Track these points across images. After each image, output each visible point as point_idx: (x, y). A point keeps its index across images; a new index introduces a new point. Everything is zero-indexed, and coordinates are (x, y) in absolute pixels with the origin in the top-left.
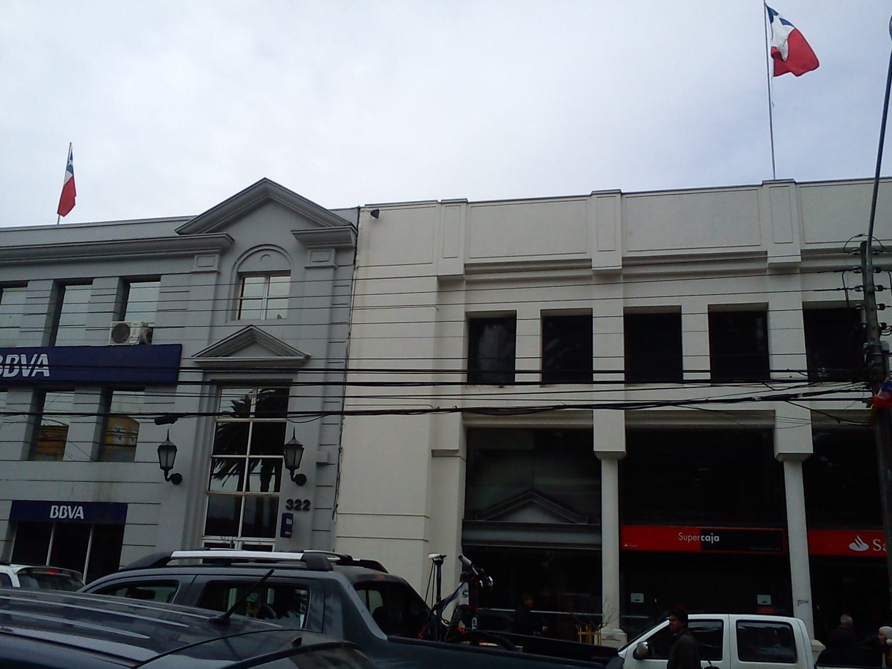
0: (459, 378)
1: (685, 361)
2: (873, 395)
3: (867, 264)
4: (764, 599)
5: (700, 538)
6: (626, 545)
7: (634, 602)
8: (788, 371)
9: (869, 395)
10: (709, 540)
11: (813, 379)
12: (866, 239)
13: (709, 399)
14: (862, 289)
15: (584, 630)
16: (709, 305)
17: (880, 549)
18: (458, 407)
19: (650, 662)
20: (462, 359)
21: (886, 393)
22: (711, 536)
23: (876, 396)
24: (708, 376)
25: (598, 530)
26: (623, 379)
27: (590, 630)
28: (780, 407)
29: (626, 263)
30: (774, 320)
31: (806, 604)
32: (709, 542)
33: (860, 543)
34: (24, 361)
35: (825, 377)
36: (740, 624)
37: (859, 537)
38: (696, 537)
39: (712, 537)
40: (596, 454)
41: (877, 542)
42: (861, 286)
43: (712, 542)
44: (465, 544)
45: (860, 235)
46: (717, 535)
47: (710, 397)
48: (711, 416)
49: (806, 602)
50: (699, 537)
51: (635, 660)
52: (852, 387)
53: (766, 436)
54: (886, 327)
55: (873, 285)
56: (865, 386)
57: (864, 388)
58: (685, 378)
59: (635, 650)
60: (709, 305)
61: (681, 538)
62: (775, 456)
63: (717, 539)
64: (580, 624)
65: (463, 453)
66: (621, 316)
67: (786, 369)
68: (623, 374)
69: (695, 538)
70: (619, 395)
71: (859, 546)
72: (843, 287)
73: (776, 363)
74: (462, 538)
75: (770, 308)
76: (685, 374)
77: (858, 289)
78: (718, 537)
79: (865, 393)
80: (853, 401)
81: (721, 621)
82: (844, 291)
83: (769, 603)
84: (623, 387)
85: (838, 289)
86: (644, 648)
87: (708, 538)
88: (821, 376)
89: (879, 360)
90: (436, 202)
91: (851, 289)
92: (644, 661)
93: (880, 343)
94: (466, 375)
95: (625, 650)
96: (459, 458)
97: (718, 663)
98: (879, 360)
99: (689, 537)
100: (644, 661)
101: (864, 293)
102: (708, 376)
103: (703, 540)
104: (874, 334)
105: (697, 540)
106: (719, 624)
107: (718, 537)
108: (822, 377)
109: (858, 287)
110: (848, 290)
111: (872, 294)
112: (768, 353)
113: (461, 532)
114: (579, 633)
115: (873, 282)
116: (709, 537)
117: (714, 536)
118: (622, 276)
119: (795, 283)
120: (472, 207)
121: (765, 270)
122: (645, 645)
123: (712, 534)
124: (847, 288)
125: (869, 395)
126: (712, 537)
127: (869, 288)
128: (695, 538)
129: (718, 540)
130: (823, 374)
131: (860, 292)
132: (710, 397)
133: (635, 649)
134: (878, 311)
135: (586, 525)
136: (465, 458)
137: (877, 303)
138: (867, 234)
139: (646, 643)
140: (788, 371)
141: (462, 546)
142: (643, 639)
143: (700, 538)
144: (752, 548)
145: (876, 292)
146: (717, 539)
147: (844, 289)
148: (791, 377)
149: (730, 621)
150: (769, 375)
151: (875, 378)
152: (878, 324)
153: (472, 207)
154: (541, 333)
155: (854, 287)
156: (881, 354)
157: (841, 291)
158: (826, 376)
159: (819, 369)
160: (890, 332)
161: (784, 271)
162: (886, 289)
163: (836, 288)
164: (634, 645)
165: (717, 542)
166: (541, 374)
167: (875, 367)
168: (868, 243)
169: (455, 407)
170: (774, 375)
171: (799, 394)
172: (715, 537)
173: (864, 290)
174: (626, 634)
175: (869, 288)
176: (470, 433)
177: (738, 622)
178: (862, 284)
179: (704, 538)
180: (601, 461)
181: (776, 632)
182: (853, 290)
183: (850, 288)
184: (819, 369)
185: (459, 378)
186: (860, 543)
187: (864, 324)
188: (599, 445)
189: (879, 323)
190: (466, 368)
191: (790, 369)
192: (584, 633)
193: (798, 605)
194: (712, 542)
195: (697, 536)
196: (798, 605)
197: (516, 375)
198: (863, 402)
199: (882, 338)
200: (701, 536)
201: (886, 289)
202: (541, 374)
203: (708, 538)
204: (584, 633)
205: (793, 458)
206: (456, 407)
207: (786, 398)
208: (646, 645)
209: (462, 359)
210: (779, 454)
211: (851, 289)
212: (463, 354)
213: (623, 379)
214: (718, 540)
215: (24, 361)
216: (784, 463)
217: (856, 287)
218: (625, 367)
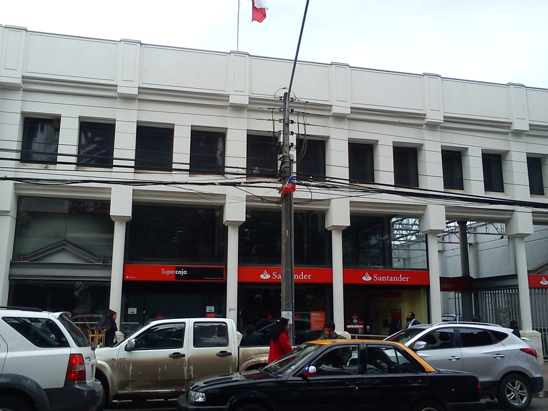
0: (14, 155)
1: (174, 156)
2: (283, 185)
3: (287, 106)
4: (210, 309)
5: (175, 272)
6: (127, 277)
7: (130, 313)
8: (237, 168)
9: (280, 185)
10: (181, 273)
11: (249, 174)
12: (287, 91)
13: (187, 182)
14: (282, 121)
15: (93, 333)
16: (393, 142)
17: (276, 277)
18: (7, 177)
19: (135, 352)
20: (17, 141)
21: (291, 184)
22: (182, 271)
23: (284, 186)
24: (188, 167)
25: (109, 267)
26: (133, 165)
27: (98, 333)
28: (229, 190)
29: (445, 119)
30: (229, 136)
31: (234, 310)
32: (180, 274)
33: (368, 276)
34: (295, 170)
35: (257, 173)
36: (196, 324)
37: (266, 271)
38: (307, 276)
39: (182, 271)
40: (111, 217)
41: (376, 276)
42: (282, 120)
43: (182, 275)
44: (10, 278)
45: (284, 88)
46: (186, 270)
47: (188, 181)
48: (412, 207)
49: (234, 309)
50: (174, 271)
51: (126, 352)
52: (272, 180)
53: (322, 215)
54: (293, 146)
55: (289, 119)
56: (279, 180)
57: (278, 181)
58: (173, 168)
59: (127, 345)
60: (393, 142)
61: (163, 272)
62: (224, 222)
63: (185, 272)
64: (90, 329)
65: (14, 213)
66: (77, 118)
67: (235, 167)
68: (134, 162)
69: (172, 272)
70: (130, 175)
71: (265, 276)
72: (272, 119)
73: (176, 158)
74: (9, 273)
75: (379, 143)
76: (173, 165)
77: (280, 121)
78: (186, 272)
79: (278, 184)
80: (271, 189)
81: (184, 323)
82: (272, 121)
83: (213, 311)
84: (246, 180)
85: (269, 120)
86: (132, 344)
87: (180, 272)
88: (255, 172)
89: (288, 165)
90: (347, 65)
91: (277, 121)
92: (132, 352)
93: (289, 155)
94: (20, 154)
95: (120, 345)
96: (10, 217)
97: (180, 350)
98: (288, 165)
99: (168, 271)
100: (132, 352)
101: (283, 124)
102: (188, 167)
103: (177, 274)
104: (287, 149)
105: (173, 274)
106: (183, 325)
107: (186, 272)
108: (256, 173)
109: (280, 120)
110: (275, 121)
111: (287, 124)
112: (225, 155)
113: (9, 269)
114: (89, 336)
115: (289, 118)
116: (181, 271)
117: (183, 271)
118: (439, 127)
119: (346, 124)
120: (234, 55)
121: (422, 125)
122: (133, 342)
123: (183, 270)
124: (274, 120)
125: (280, 185)
126: (182, 271)
127: (286, 121)
128: (172, 272)
129: (186, 273)
130: (256, 171)
131: (281, 123)
132: (188, 181)
133: (126, 344)
134: (290, 135)
135: (102, 264)
136: (15, 217)
137: (290, 131)
138: (288, 88)
139: (134, 340)
140: (237, 168)
141: (9, 279)
142: (132, 338)
143: (175, 272)
144: (206, 278)
145: (290, 124)
146: (185, 272)
147: (304, 124)
148: (238, 171)
149: (189, 323)
150: (224, 169)
151: (285, 175)
152: (289, 143)
153: (234, 55)
154: (79, 128)
155: (278, 119)
156: (289, 161)
157: (271, 121)
158: (258, 172)
159: (255, 168)
160: (295, 149)
161: (433, 126)
162: (295, 123)
163: (268, 119)
164: (126, 342)
165: (185, 275)
166: (77, 157)
167: (285, 169)
168: (288, 94)
169: (5, 177)
170: (227, 170)
171: (242, 182)
172: (185, 271)
173: (283, 122)
174: (124, 334)
175: (286, 121)
176: (20, 199)
177: (195, 323)
178: (283, 119)
179: (177, 272)
180: (114, 222)
181: (217, 328)
182: (277, 121)
183: (276, 120)
184: (255, 168)
185: (14, 155)
186: (368, 276)
187: (282, 142)
188: (114, 212)
189: (290, 143)
190: (20, 149)
191: (238, 167)
192: (93, 336)
193: (229, 311)
194: (182, 275)
195: (308, 275)
196: (229, 311)
197: (114, 160)
198: (277, 190)
199: (290, 152)
200: (176, 271)
201: (295, 123)
202: (77, 157)
203: (180, 272)
204: (93, 336)
205: (233, 223)
206: (6, 176)
207: (234, 184)
208: (134, 341)
209: (17, 141)
210: (226, 221)
211: (277, 121)
212: (77, 144)
213: (133, 165)
214: (186, 273)
215: (295, 170)
216: (332, 231)
217: (279, 120)
218: (136, 158)
